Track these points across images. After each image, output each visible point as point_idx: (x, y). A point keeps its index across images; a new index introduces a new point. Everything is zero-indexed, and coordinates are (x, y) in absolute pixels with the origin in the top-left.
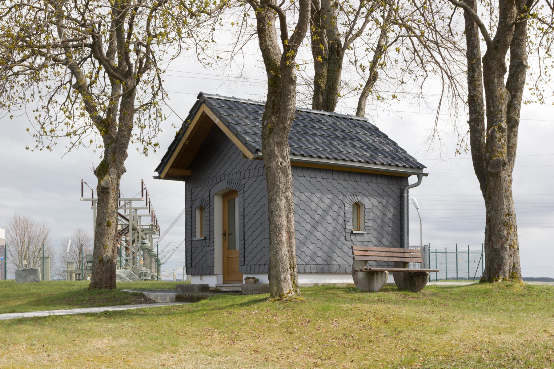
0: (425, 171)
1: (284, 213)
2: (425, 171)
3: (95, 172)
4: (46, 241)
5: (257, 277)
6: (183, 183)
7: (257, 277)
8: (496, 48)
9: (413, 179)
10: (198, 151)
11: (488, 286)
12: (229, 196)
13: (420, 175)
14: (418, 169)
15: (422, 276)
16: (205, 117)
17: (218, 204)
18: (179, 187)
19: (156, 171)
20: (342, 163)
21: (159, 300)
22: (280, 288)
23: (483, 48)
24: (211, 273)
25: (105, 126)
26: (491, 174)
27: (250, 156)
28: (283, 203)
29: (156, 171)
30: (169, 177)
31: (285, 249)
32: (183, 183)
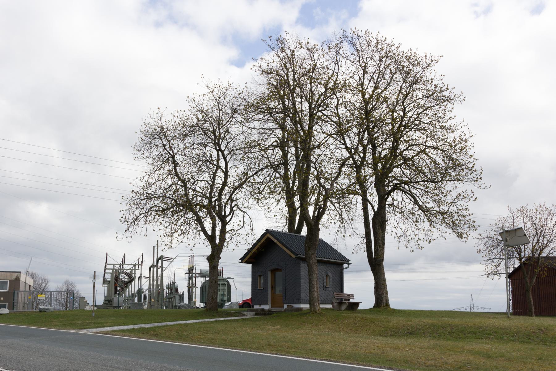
0: (350, 262)
1: (315, 280)
2: (350, 262)
3: (207, 259)
4: (47, 285)
5: (292, 305)
6: (250, 265)
7: (292, 305)
8: (377, 215)
9: (345, 266)
10: (263, 253)
11: (378, 309)
12: (274, 271)
13: (349, 264)
14: (348, 261)
15: (357, 304)
16: (268, 238)
17: (270, 274)
18: (248, 267)
19: (244, 260)
20: (333, 260)
21: (248, 315)
22: (315, 308)
23: (371, 213)
24: (266, 303)
25: (211, 239)
26: (378, 264)
27: (294, 256)
28: (315, 276)
29: (244, 260)
30: (246, 262)
31: (316, 294)
32: (250, 265)
